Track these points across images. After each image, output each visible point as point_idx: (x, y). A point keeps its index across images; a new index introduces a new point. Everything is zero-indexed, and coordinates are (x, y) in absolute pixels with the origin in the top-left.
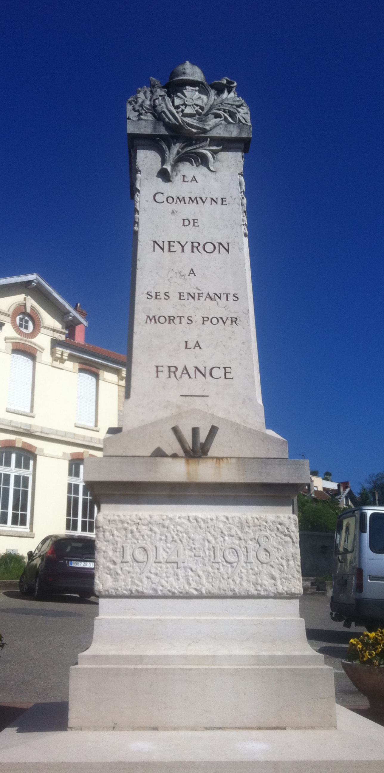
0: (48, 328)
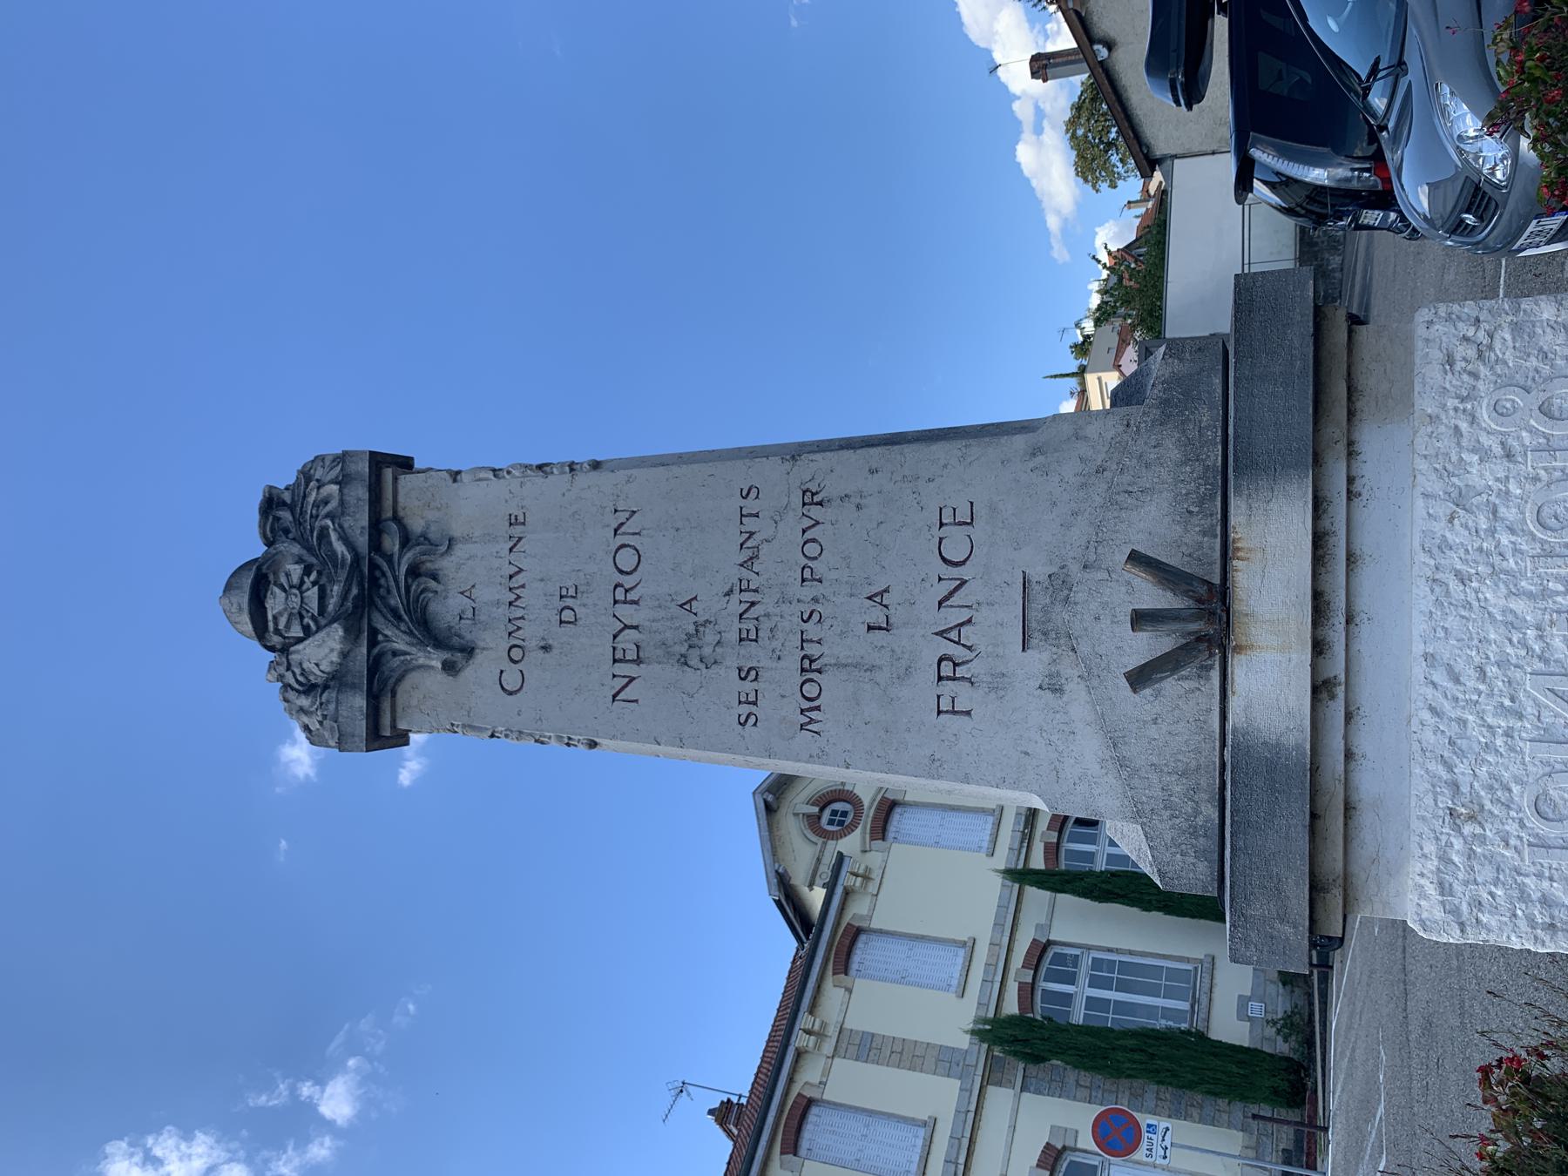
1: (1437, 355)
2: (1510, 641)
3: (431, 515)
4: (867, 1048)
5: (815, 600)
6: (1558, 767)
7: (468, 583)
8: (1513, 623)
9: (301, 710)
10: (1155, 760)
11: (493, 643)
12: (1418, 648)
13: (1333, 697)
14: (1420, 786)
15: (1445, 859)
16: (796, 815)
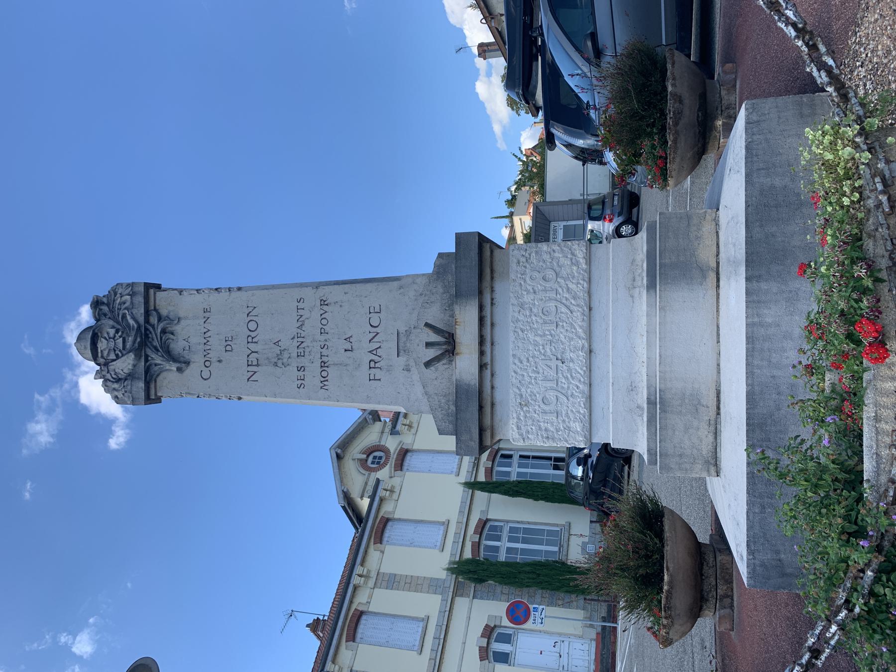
0: (381, 438)
1: (515, 261)
3: (171, 308)
4: (392, 582)
5: (326, 340)
7: (186, 335)
8: (536, 344)
9: (114, 389)
11: (197, 360)
12: (511, 353)
14: (512, 396)
15: (519, 418)
16: (354, 460)
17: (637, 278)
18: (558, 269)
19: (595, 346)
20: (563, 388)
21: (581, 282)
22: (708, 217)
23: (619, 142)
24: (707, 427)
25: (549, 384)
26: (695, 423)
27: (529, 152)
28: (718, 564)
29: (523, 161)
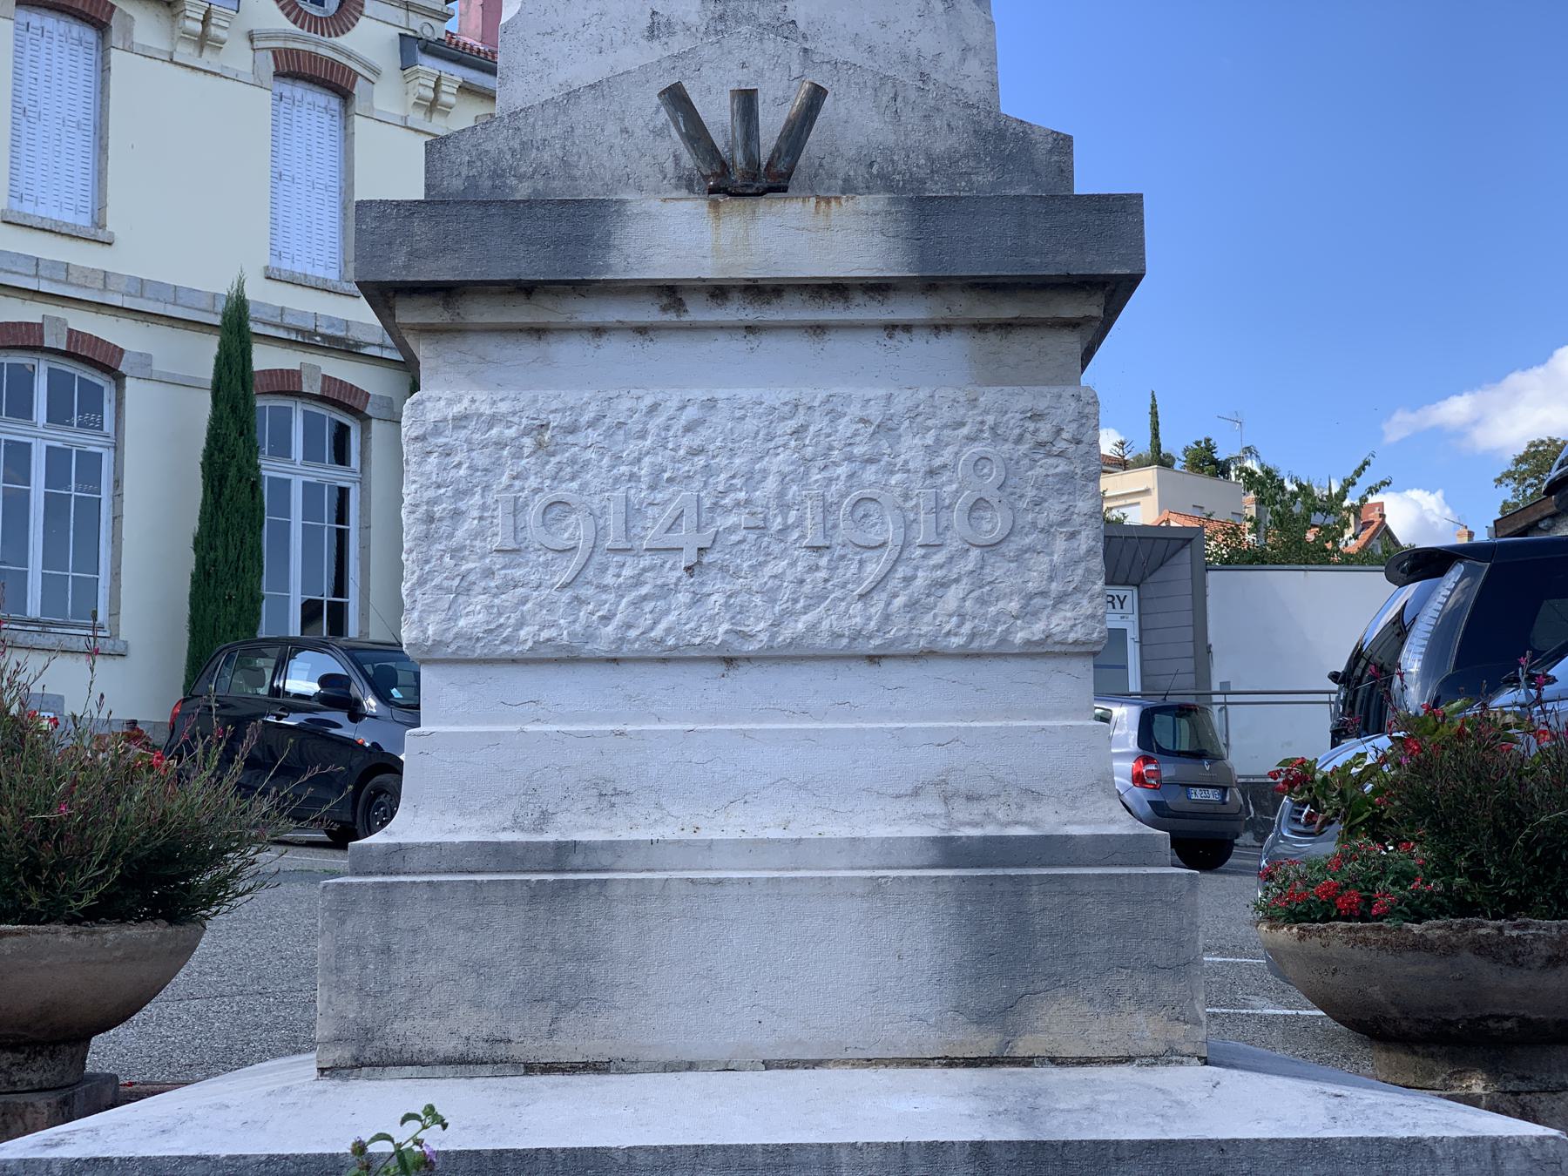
1: (1042, 405)
2: (733, 477)
6: (601, 522)
8: (752, 478)
10: (579, 131)
12: (721, 394)
13: (664, 309)
14: (571, 397)
15: (493, 420)
17: (977, 810)
18: (1010, 549)
19: (746, 678)
20: (603, 569)
21: (967, 628)
22: (1181, 1029)
23: (1423, 768)
24: (485, 1033)
25: (614, 523)
26: (495, 995)
27: (1373, 516)
28: (20, 1099)
29: (1342, 495)
